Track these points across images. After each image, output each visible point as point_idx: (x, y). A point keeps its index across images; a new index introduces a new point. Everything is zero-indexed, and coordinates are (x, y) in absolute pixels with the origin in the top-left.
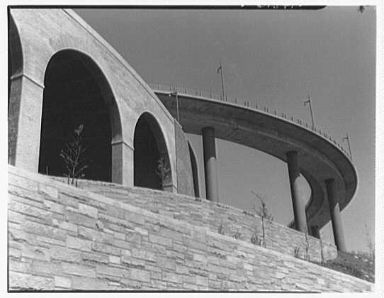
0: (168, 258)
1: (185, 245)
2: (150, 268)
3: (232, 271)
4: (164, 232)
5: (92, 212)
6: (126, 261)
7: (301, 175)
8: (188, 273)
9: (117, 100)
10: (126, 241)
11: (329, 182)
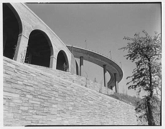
0: (43, 84)
1: (50, 81)
2: (34, 87)
3: (68, 91)
4: (42, 76)
5: (14, 67)
6: (25, 83)
7: (107, 71)
8: (50, 90)
9: (53, 45)
10: (26, 77)
11: (115, 74)
